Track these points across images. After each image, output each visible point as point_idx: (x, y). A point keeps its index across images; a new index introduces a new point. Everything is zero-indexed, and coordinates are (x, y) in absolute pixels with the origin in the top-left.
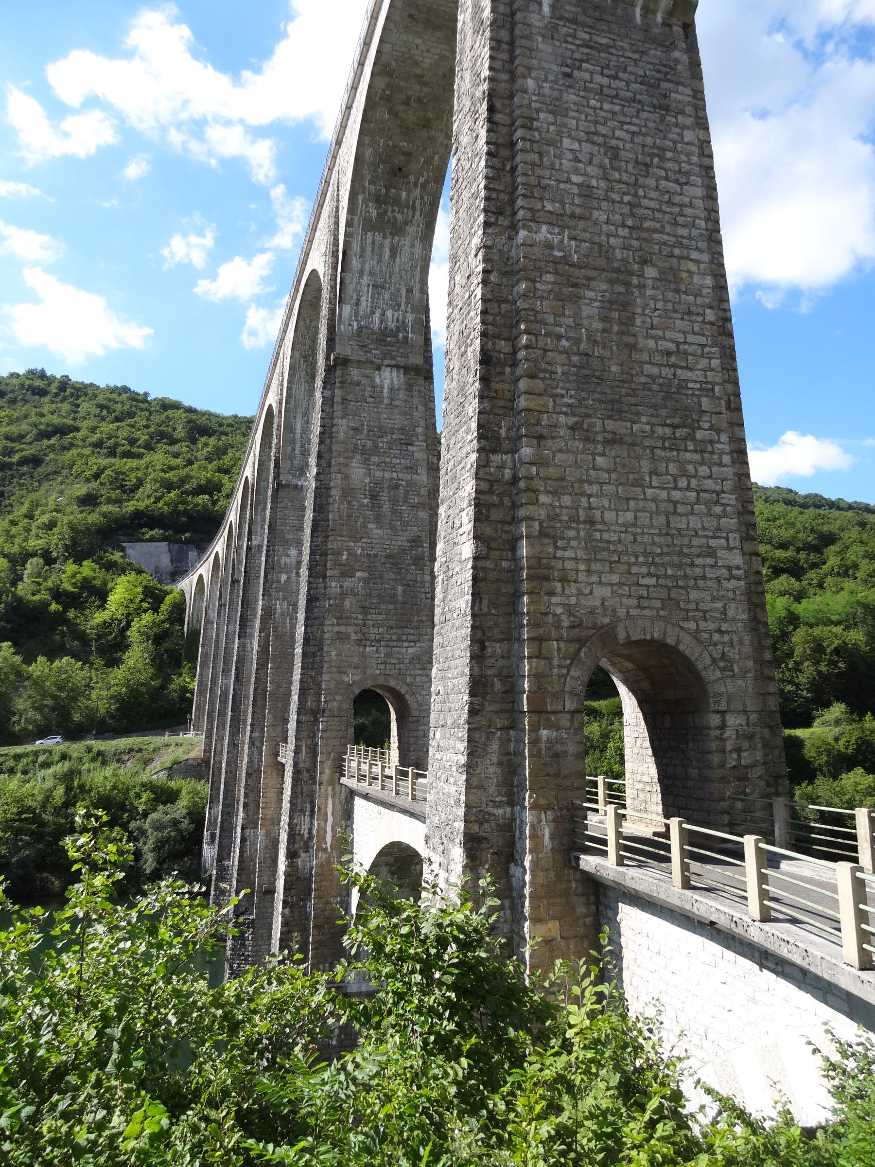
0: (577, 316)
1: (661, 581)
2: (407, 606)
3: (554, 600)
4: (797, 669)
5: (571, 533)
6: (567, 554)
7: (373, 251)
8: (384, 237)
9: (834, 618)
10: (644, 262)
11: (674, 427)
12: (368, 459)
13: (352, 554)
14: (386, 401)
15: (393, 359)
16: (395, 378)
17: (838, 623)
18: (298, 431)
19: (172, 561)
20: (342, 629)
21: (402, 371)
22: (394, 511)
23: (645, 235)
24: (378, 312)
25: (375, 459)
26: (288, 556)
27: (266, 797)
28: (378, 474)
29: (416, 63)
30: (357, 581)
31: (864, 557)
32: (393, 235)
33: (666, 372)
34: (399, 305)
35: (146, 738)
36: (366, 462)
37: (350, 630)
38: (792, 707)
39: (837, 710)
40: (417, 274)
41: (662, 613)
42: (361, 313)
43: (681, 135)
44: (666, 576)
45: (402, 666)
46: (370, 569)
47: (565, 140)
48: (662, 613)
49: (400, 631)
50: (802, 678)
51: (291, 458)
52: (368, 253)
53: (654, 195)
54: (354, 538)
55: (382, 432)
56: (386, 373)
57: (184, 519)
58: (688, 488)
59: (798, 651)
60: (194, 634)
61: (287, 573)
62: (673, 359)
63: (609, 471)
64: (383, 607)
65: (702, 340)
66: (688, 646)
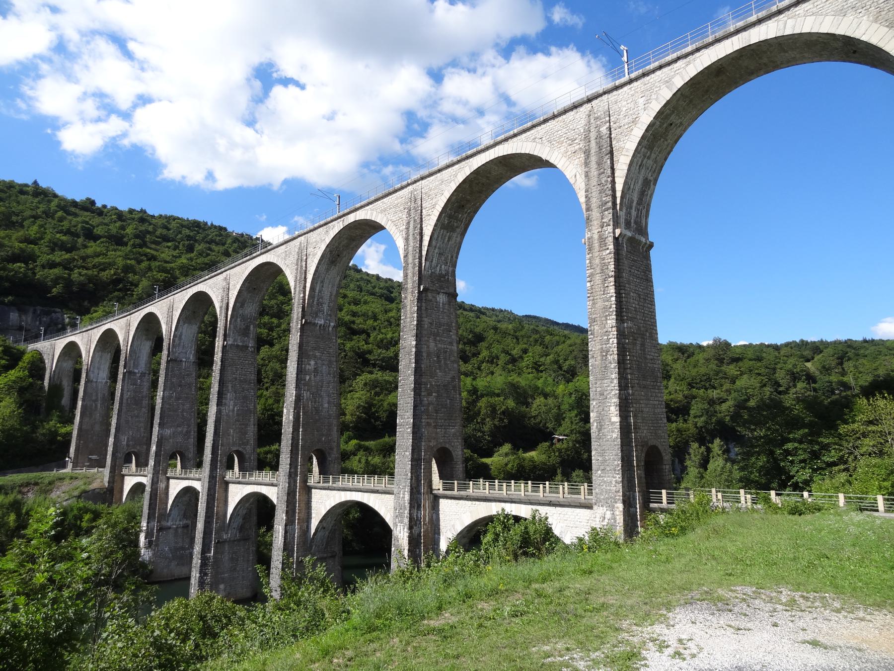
4: (483, 423)
9: (497, 391)
13: (431, 385)
17: (498, 395)
18: (317, 291)
20: (429, 420)
22: (446, 364)
25: (438, 338)
26: (310, 364)
27: (303, 505)
29: (490, 173)
30: (433, 398)
31: (502, 352)
36: (435, 340)
37: (432, 421)
39: (506, 448)
40: (456, 250)
46: (438, 392)
50: (486, 428)
52: (440, 238)
54: (432, 377)
56: (441, 296)
57: (7, 284)
59: (483, 411)
66: (660, 447)
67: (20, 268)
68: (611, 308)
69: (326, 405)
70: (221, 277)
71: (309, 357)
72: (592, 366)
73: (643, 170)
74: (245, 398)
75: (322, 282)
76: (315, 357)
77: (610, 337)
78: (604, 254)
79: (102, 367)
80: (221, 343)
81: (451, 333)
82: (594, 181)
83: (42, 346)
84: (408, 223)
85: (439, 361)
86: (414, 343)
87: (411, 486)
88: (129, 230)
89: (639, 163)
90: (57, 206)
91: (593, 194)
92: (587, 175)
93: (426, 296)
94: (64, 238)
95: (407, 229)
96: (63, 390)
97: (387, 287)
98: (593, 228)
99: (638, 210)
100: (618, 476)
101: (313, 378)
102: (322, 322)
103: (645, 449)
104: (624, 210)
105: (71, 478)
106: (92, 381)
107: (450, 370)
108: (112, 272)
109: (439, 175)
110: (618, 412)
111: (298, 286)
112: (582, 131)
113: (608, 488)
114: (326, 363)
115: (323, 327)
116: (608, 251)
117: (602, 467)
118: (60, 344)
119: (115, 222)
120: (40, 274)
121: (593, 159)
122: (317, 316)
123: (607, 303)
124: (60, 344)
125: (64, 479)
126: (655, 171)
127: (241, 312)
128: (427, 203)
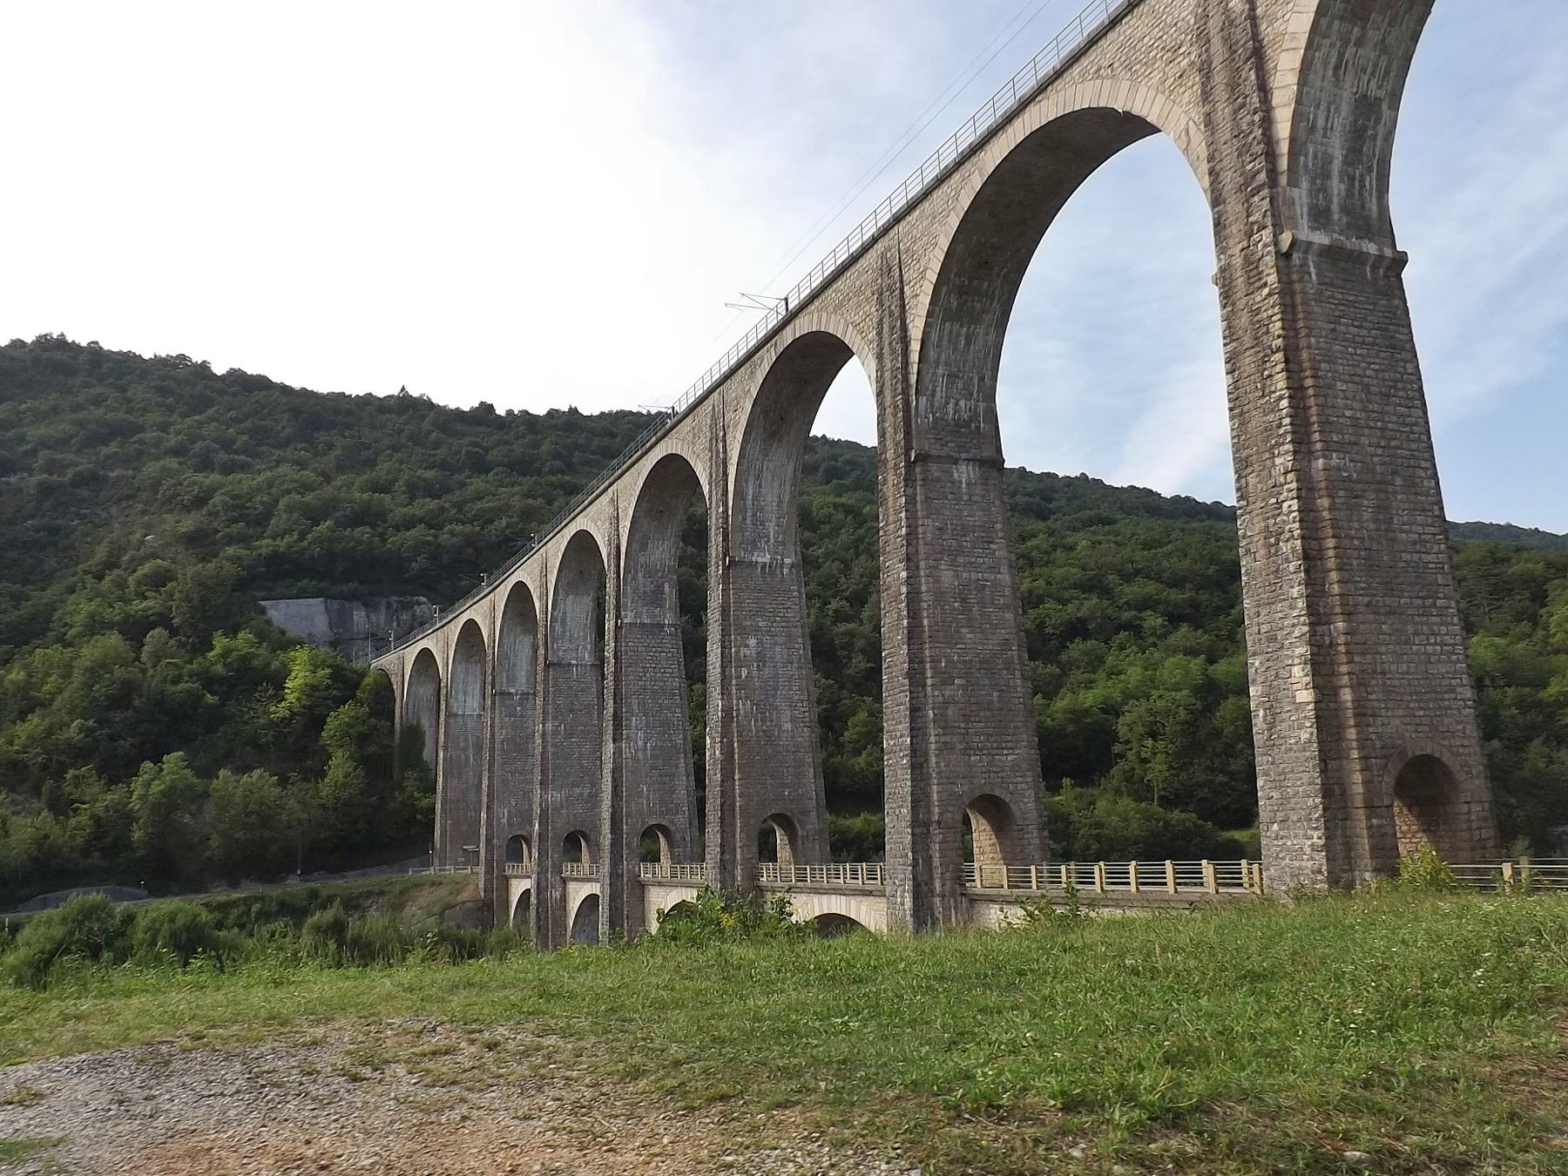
0: (1360, 521)
1: (1427, 713)
2: (1004, 712)
3: (1371, 729)
5: (1374, 682)
6: (1373, 697)
7: (949, 340)
8: (961, 326)
10: (1395, 473)
11: (1423, 598)
12: (955, 561)
13: (950, 661)
14: (965, 497)
15: (968, 452)
16: (971, 472)
19: (331, 626)
20: (948, 739)
21: (977, 463)
23: (1392, 452)
24: (952, 401)
25: (961, 560)
26: (747, 646)
28: (964, 575)
30: (955, 690)
32: (970, 323)
33: (1415, 557)
34: (972, 395)
35: (385, 877)
36: (953, 563)
37: (955, 739)
38: (1225, 803)
41: (1430, 735)
42: (936, 404)
43: (1404, 367)
44: (1429, 709)
45: (1004, 774)
47: (1338, 384)
48: (1430, 735)
49: (999, 739)
51: (742, 530)
52: (945, 343)
53: (1394, 419)
55: (965, 531)
58: (1436, 644)
60: (414, 735)
61: (748, 667)
62: (1418, 547)
63: (1390, 635)
64: (982, 714)
65: (1432, 530)
67: (363, 533)
68: (1280, 426)
69: (788, 726)
70: (605, 499)
71: (743, 632)
72: (1247, 574)
73: (1349, 79)
74: (665, 724)
75: (758, 477)
76: (757, 629)
77: (1281, 498)
78: (1259, 299)
79: (470, 689)
80: (612, 623)
81: (993, 546)
82: (1225, 134)
83: (387, 661)
84: (880, 323)
85: (966, 610)
86: (904, 574)
87: (914, 879)
88: (546, 447)
89: (1333, 61)
90: (433, 424)
91: (1225, 163)
92: (1209, 121)
93: (923, 472)
94: (430, 474)
95: (879, 334)
96: (423, 734)
97: (1042, 490)
98: (1231, 242)
99: (1352, 179)
100: (1316, 834)
101: (755, 673)
102: (767, 558)
103: (1395, 767)
104: (1305, 184)
105: (433, 884)
106: (456, 715)
107: (995, 627)
108: (504, 522)
109: (926, 204)
110: (1308, 679)
111: (714, 492)
112: (1192, 22)
113: (1297, 864)
114: (780, 640)
115: (770, 569)
116: (1266, 291)
117: (1280, 816)
118: (411, 653)
119: (524, 437)
120: (394, 539)
121: (1219, 78)
122: (755, 547)
123: (1271, 417)
124: (411, 653)
125: (424, 885)
126: (1387, 73)
127: (642, 560)
128: (911, 271)
